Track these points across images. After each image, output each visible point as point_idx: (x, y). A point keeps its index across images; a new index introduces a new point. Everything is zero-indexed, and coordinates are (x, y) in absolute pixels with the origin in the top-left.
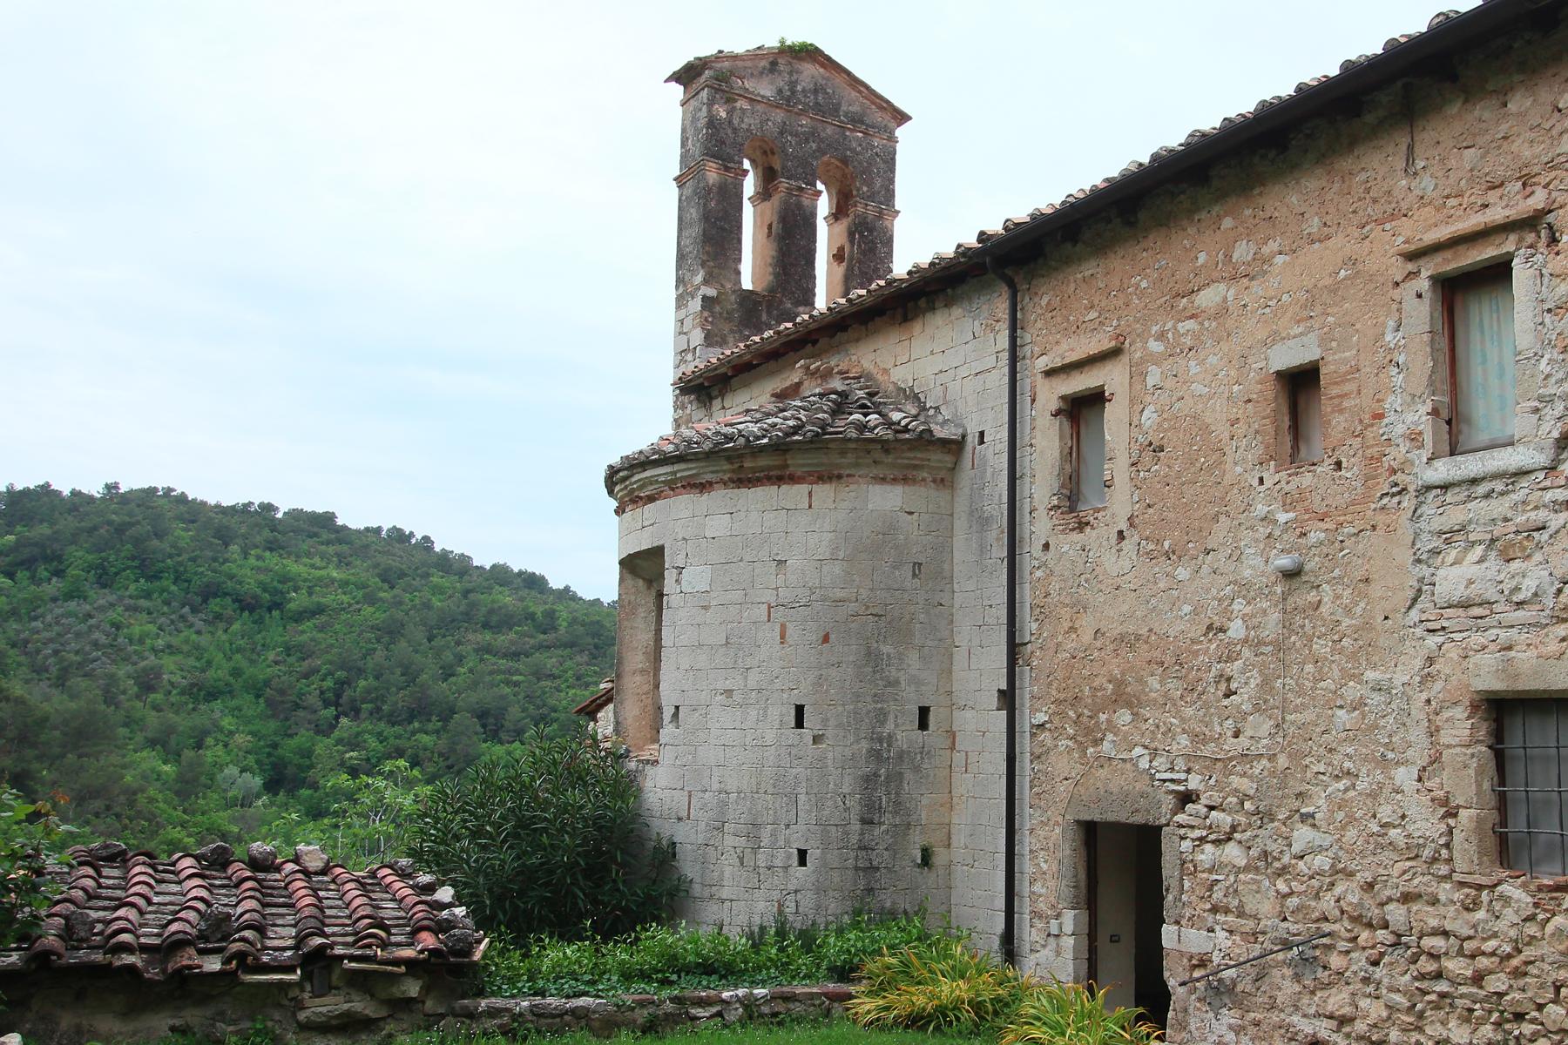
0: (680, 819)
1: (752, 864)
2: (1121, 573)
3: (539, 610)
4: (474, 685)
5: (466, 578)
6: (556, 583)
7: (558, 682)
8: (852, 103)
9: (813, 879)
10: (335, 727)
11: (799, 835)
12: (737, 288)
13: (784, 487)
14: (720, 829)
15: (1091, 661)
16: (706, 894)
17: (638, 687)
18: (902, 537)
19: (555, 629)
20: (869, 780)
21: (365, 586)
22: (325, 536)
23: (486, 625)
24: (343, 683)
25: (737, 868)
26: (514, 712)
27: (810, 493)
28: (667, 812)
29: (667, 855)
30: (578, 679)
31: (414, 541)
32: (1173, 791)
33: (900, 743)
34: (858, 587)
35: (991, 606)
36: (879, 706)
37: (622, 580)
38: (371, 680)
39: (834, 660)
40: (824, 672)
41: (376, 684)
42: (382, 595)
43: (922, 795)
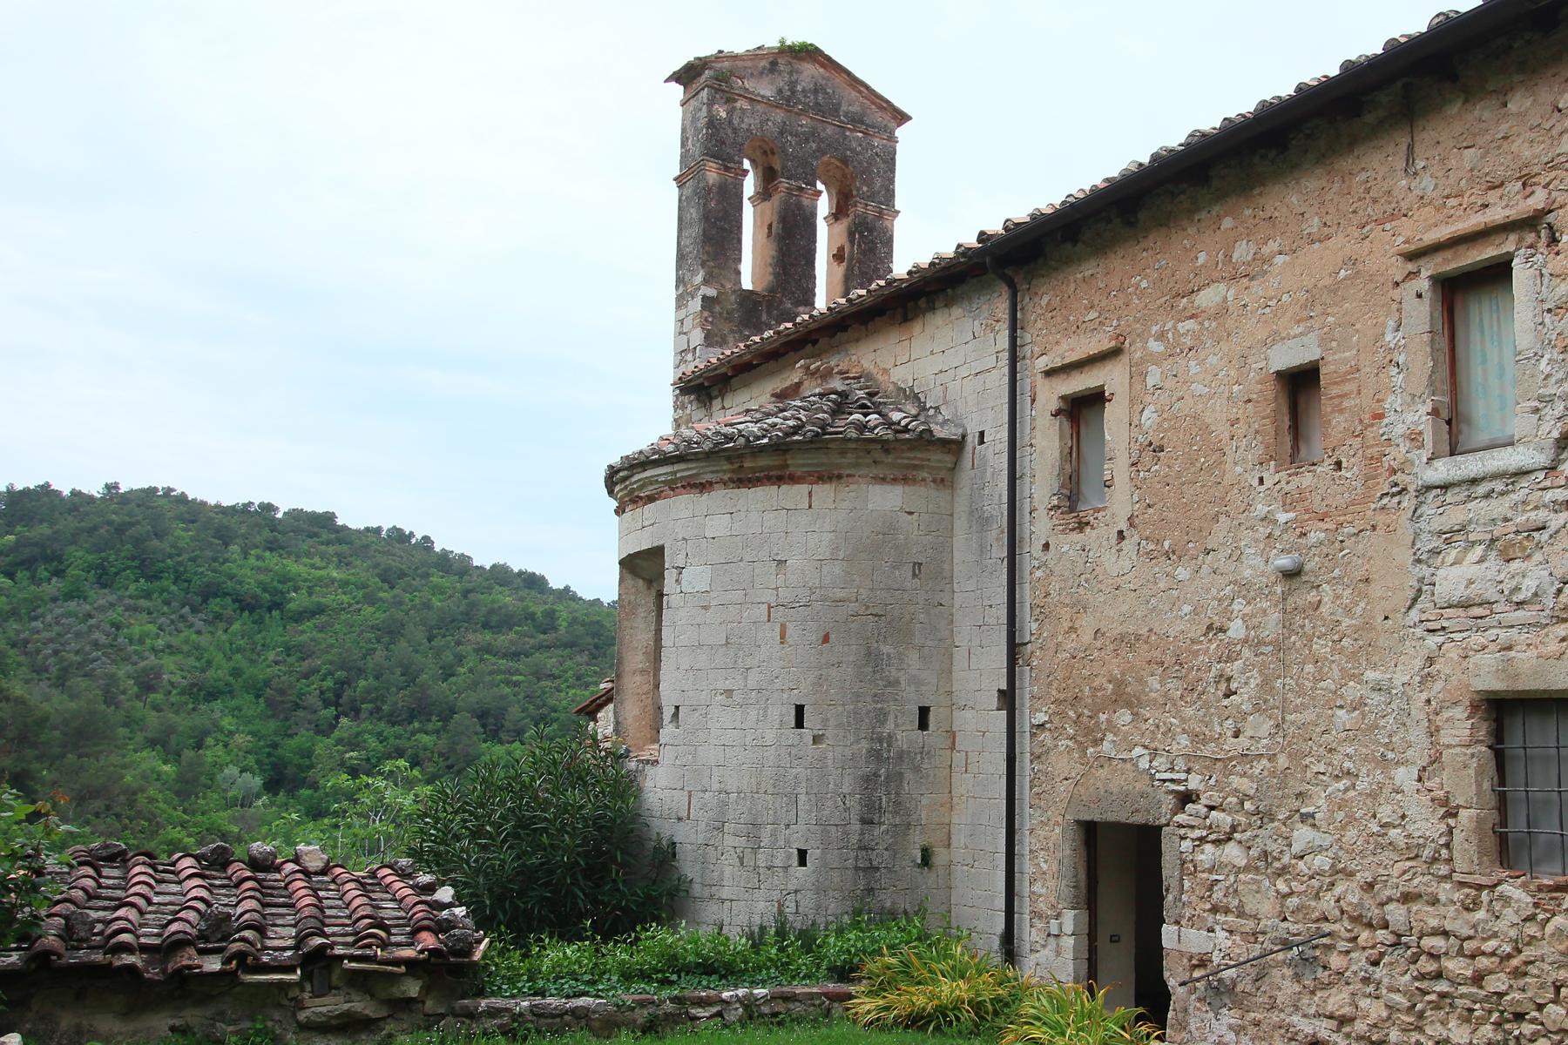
0: (680, 819)
1: (752, 864)
2: (1121, 573)
3: (539, 610)
4: (474, 685)
5: (466, 578)
6: (556, 583)
7: (558, 682)
8: (852, 103)
9: (813, 879)
10: (335, 727)
11: (799, 835)
12: (737, 288)
13: (784, 487)
14: (720, 829)
15: (1091, 661)
16: (706, 894)
18: (902, 537)
19: (555, 629)
20: (869, 780)
22: (325, 536)
23: (486, 625)
24: (343, 683)
25: (737, 868)
26: (514, 712)
27: (810, 493)
28: (667, 812)
29: (667, 855)
30: (578, 679)
31: (414, 541)
32: (1173, 791)
33: (900, 743)
34: (858, 587)
35: (991, 606)
36: (879, 706)
37: (622, 580)
38: (371, 680)
39: (834, 660)
40: (824, 672)
41: (376, 684)
42: (382, 595)
43: (922, 795)
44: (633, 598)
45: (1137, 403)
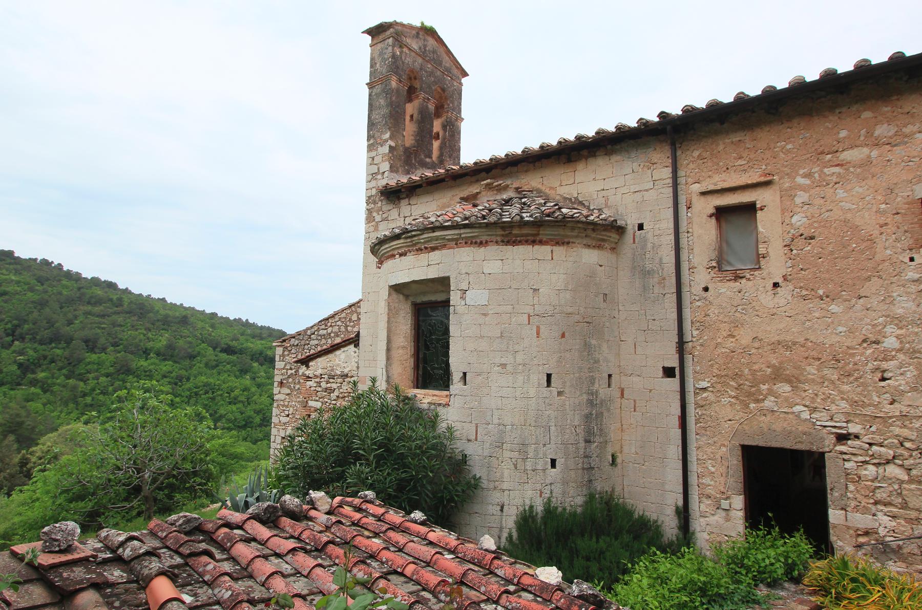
0: (469, 440)
1: (523, 468)
2: (777, 306)
3: (115, 297)
4: (83, 328)
5: (79, 282)
6: (122, 286)
7: (123, 328)
8: (447, 62)
10: (11, 345)
11: (552, 450)
13: (536, 247)
15: (750, 354)
16: (491, 485)
17: (401, 356)
18: (598, 279)
19: (122, 305)
20: (588, 417)
21: (29, 284)
22: (9, 261)
23: (89, 303)
24: (16, 326)
26: (102, 340)
29: (461, 463)
30: (133, 326)
31: (53, 265)
32: (833, 433)
34: (579, 306)
35: (654, 320)
36: (591, 374)
37: (390, 294)
38: (31, 325)
40: (562, 354)
41: (33, 327)
42: (37, 288)
44: (396, 305)
45: (787, 211)
